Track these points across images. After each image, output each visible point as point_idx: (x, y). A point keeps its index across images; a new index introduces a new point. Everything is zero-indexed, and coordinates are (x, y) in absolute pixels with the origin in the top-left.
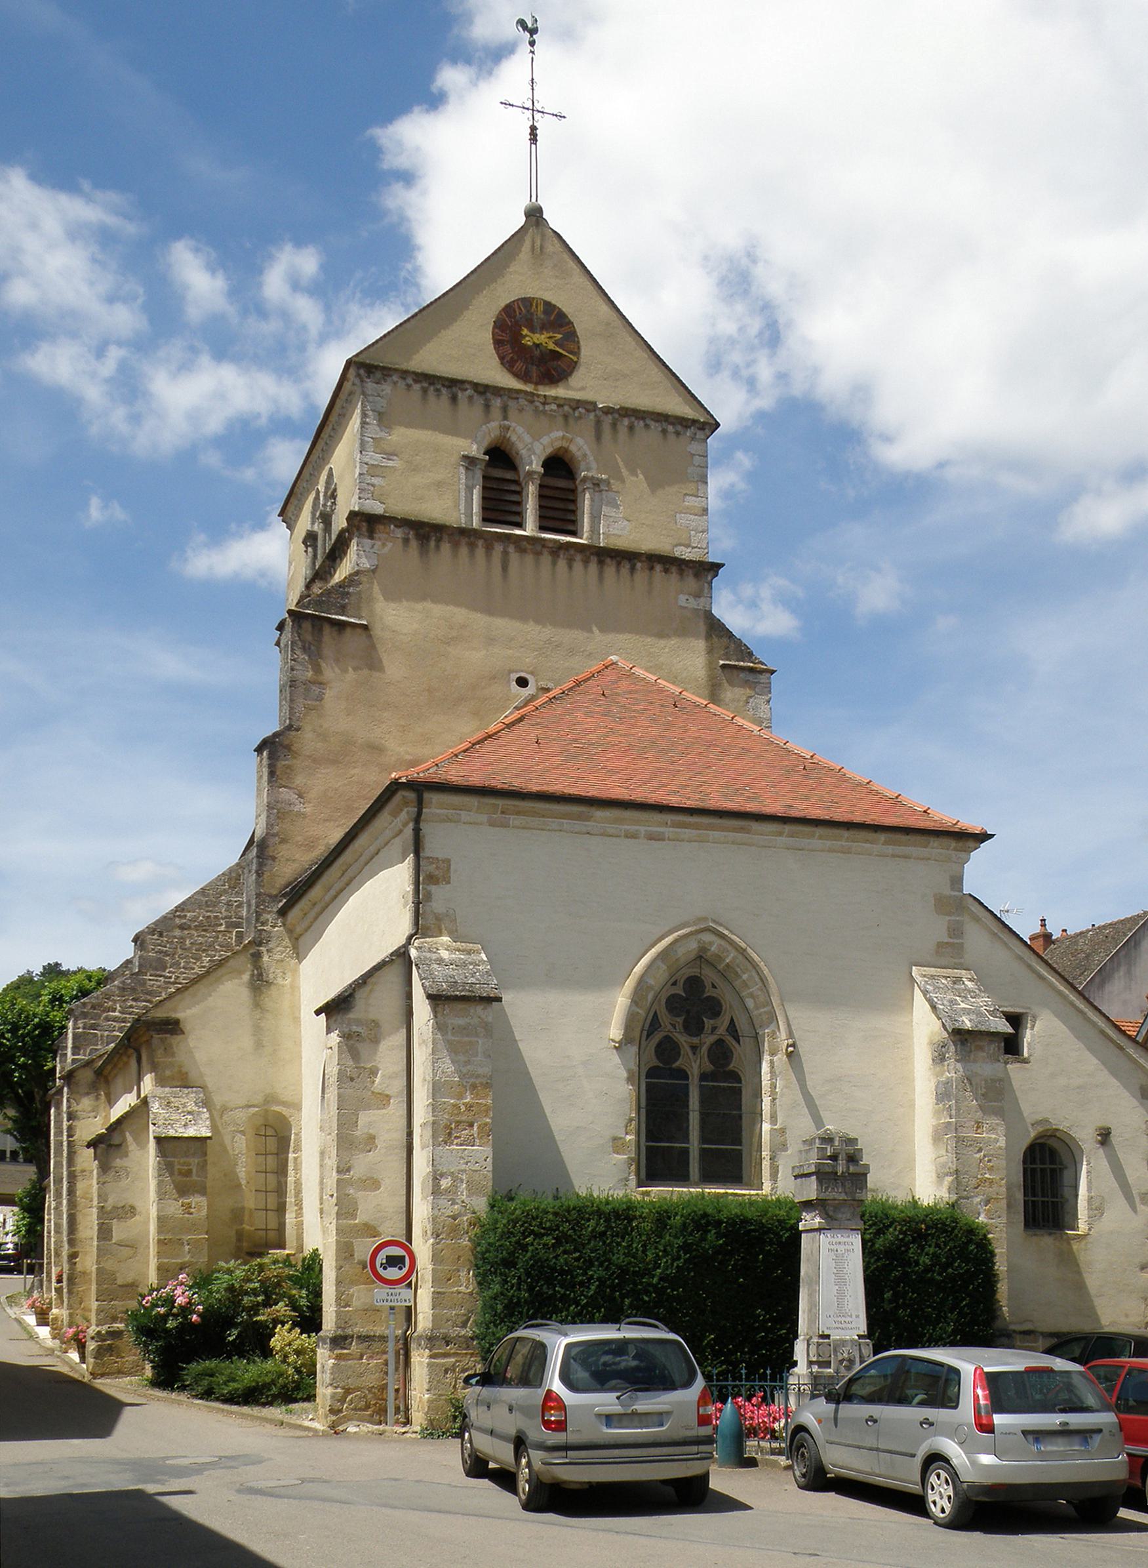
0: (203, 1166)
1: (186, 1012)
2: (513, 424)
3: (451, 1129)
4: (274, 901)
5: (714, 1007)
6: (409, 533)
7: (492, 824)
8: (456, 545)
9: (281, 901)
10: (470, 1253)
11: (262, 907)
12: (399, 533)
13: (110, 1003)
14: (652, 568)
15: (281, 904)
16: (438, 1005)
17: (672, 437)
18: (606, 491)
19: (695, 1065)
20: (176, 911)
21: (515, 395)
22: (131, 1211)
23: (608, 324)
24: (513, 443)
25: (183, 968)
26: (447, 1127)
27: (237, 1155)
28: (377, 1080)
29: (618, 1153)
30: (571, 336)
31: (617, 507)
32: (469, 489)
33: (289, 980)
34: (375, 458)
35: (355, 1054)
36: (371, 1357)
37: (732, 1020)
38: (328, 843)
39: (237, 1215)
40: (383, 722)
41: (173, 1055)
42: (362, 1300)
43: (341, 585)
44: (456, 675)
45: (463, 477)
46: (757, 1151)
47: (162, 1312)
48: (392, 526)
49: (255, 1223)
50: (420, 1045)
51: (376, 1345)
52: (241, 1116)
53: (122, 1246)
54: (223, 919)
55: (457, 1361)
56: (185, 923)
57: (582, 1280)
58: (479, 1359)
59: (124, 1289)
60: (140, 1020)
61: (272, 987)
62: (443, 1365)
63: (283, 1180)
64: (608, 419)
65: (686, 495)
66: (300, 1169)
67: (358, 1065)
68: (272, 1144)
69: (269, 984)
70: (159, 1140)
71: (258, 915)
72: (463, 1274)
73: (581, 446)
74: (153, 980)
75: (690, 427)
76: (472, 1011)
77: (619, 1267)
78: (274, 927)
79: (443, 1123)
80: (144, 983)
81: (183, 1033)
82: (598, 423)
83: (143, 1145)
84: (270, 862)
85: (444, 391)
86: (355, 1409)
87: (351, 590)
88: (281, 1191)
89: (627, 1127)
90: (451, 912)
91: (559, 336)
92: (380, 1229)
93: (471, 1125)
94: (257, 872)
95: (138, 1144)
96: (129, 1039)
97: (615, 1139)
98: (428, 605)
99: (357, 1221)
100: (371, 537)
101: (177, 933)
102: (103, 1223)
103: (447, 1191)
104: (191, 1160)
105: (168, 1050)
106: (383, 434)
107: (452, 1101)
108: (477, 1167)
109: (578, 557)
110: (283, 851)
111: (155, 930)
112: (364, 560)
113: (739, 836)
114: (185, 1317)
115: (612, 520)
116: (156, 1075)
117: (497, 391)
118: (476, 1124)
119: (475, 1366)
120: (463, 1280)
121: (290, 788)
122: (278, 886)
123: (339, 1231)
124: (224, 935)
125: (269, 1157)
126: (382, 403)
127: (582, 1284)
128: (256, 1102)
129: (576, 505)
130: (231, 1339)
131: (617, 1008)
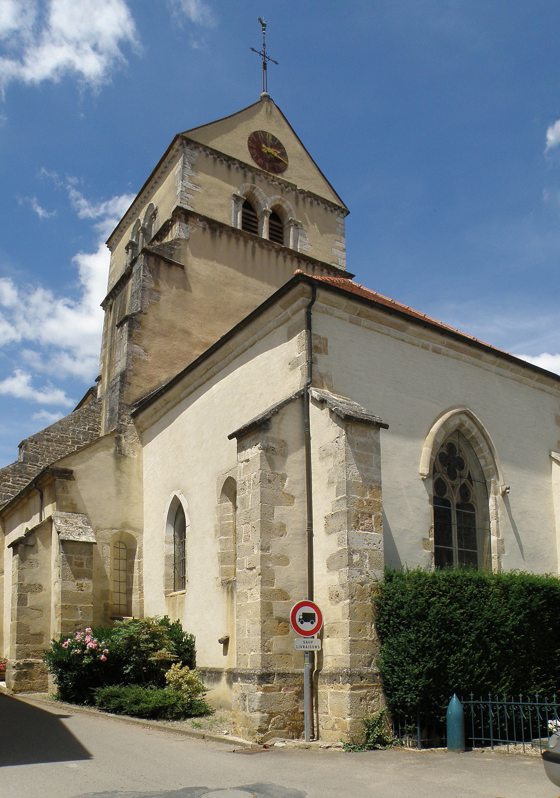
0: (90, 561)
1: (77, 467)
2: (257, 187)
3: (359, 518)
4: (129, 409)
5: (461, 464)
6: (206, 225)
7: (351, 322)
8: (229, 237)
9: (133, 409)
10: (372, 611)
11: (122, 411)
12: (201, 224)
13: (7, 477)
14: (322, 270)
15: (133, 411)
16: (348, 425)
17: (329, 212)
18: (301, 229)
19: (455, 498)
20: (45, 431)
21: (259, 173)
22: (40, 588)
23: (300, 154)
24: (256, 197)
25: (48, 462)
26: (356, 516)
27: (105, 558)
28: (286, 484)
29: (425, 549)
30: (284, 154)
31: (306, 238)
32: (236, 213)
33: (137, 456)
34: (190, 185)
35: (271, 464)
36: (287, 689)
37: (469, 473)
38: (160, 380)
39: (105, 594)
40: (191, 320)
41: (68, 492)
42: (279, 647)
43: (170, 243)
44: (229, 302)
45: (233, 205)
46: (488, 553)
47: (78, 653)
48: (198, 220)
49: (115, 600)
50: (322, 459)
51: (290, 680)
52: (108, 534)
53: (33, 609)
54: (70, 438)
55: (368, 692)
56: (50, 438)
57: (466, 630)
58: (381, 690)
59: (34, 637)
60: (49, 468)
61: (127, 459)
62: (359, 695)
63: (130, 575)
64: (301, 197)
65: (336, 240)
66: (142, 569)
67: (274, 472)
68: (123, 553)
69: (125, 456)
70: (63, 542)
71: (120, 415)
72: (368, 626)
73: (288, 205)
74: (31, 467)
75: (337, 210)
76: (368, 434)
77: (488, 620)
78: (128, 423)
79: (353, 513)
80: (26, 468)
81: (75, 480)
82: (297, 197)
83: (47, 545)
84: (127, 385)
85: (224, 162)
86: (276, 729)
87: (175, 247)
88: (129, 581)
89: (430, 532)
90: (329, 374)
91: (279, 152)
92: (290, 594)
93: (370, 516)
94: (120, 390)
95: (44, 546)
96: (35, 484)
97: (424, 539)
98: (215, 263)
99: (274, 588)
100: (186, 223)
101: (45, 443)
102: (21, 594)
103: (357, 564)
104: (83, 557)
105: (65, 489)
106: (193, 174)
107: (359, 497)
108: (374, 547)
109: (289, 257)
110: (135, 381)
111: (33, 440)
112: (182, 234)
113: (476, 361)
114: (95, 657)
115: (303, 243)
116: (57, 504)
117: (250, 168)
118: (373, 516)
119: (378, 695)
120: (368, 631)
121: (140, 346)
122: (131, 400)
123: (263, 594)
124: (70, 447)
125: (121, 561)
126: (194, 160)
127: (466, 632)
128: (116, 526)
129: (283, 235)
130: (127, 671)
131: (423, 453)
